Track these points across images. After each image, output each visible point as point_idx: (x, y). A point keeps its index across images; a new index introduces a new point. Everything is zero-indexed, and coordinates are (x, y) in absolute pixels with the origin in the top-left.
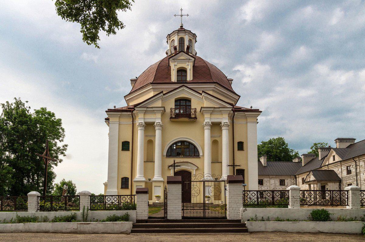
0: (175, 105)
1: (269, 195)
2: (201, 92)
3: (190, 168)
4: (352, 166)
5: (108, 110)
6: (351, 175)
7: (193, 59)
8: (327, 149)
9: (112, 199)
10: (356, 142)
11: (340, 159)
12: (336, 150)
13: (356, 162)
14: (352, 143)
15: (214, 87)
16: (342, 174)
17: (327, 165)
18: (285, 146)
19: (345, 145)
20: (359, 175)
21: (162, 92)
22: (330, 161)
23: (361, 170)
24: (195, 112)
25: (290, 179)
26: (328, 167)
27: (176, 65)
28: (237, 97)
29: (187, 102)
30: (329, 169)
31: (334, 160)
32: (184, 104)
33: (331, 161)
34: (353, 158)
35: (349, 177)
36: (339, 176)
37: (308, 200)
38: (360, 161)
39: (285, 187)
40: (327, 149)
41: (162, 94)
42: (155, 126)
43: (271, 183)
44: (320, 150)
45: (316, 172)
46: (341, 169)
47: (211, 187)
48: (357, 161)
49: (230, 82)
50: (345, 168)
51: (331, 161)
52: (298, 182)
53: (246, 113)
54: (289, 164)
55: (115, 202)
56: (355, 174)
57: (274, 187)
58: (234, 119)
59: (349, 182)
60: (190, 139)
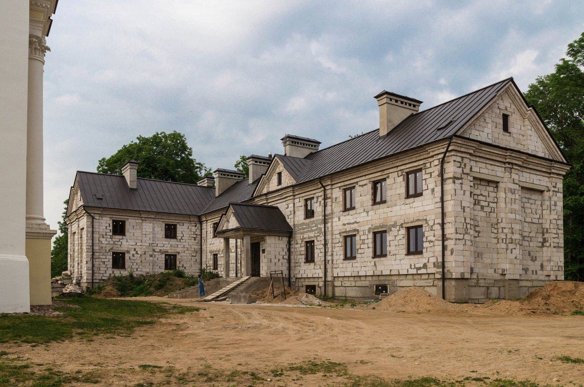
4: (315, 200)
6: (314, 221)
8: (265, 161)
10: (321, 148)
11: (293, 182)
12: (283, 158)
13: (325, 190)
14: (314, 151)
16: (294, 218)
17: (266, 194)
18: (187, 153)
19: (301, 153)
20: (330, 221)
22: (271, 185)
23: (335, 210)
25: (188, 225)
26: (267, 199)
30: (270, 204)
31: (280, 183)
33: (273, 185)
34: (321, 179)
35: (308, 225)
36: (288, 221)
38: (334, 187)
39: (178, 243)
40: (265, 161)
43: (144, 230)
44: (251, 162)
45: (242, 209)
46: (294, 204)
47: (204, 284)
48: (327, 188)
50: (302, 203)
51: (273, 185)
52: (204, 231)
54: (190, 188)
56: (321, 218)
57: (151, 242)
59: (309, 238)
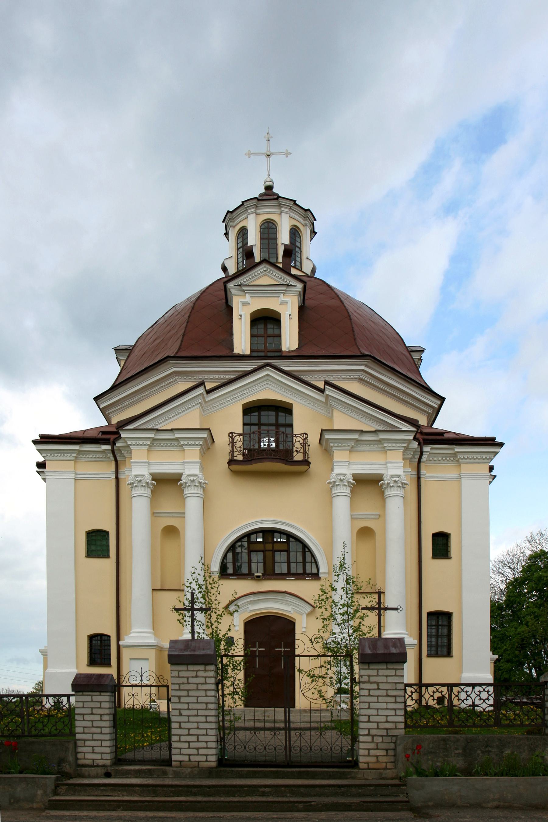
0: (244, 424)
1: (484, 695)
2: (321, 385)
3: (289, 608)
5: (42, 436)
7: (300, 286)
9: (473, 696)
15: (363, 371)
21: (202, 384)
24: (305, 443)
27: (249, 304)
28: (435, 403)
29: (280, 414)
32: (272, 420)
37: (66, 728)
41: (201, 390)
42: (181, 485)
49: (416, 357)
53: (458, 449)
55: (484, 705)
58: (422, 465)
60: (291, 526)
